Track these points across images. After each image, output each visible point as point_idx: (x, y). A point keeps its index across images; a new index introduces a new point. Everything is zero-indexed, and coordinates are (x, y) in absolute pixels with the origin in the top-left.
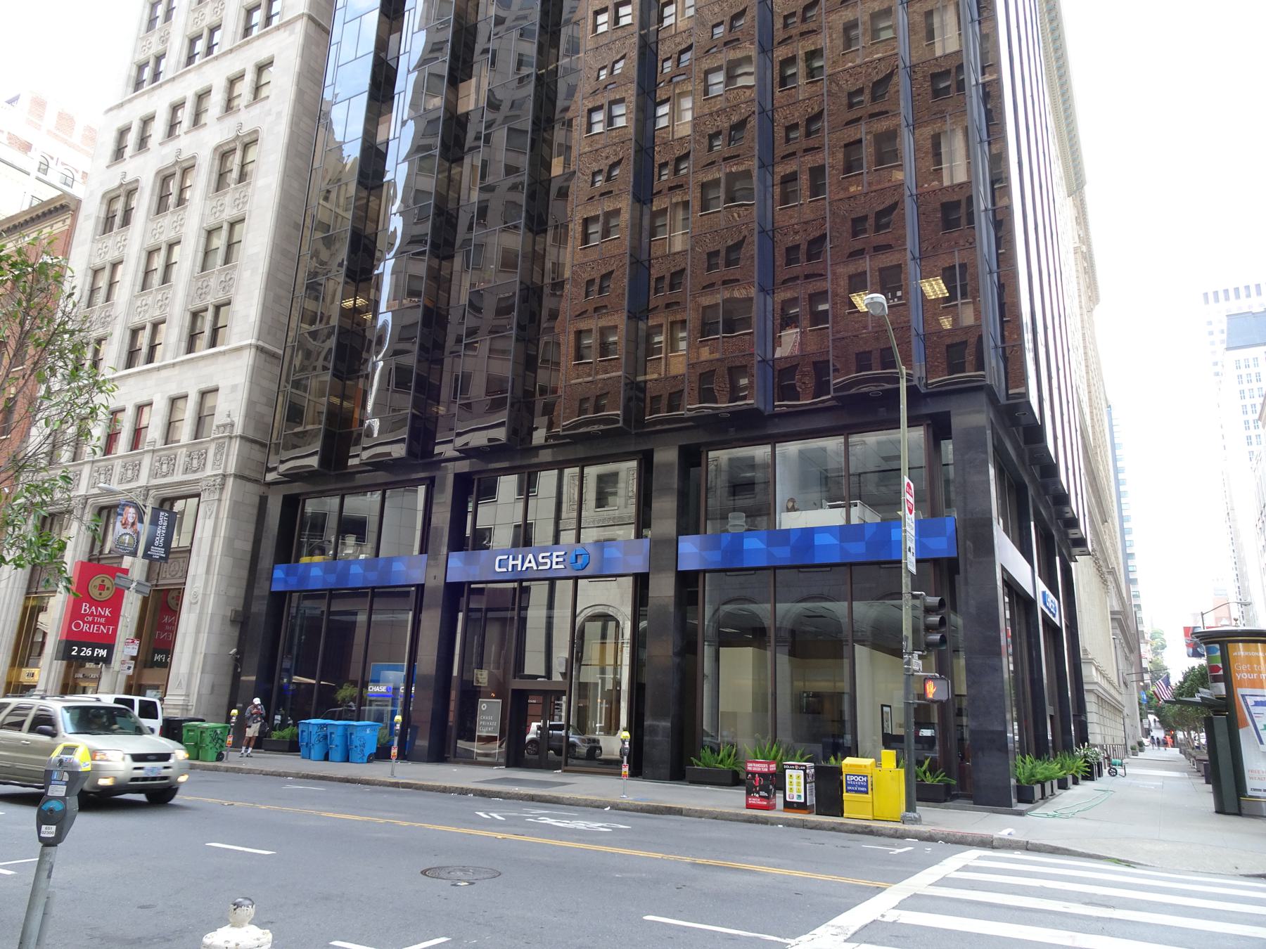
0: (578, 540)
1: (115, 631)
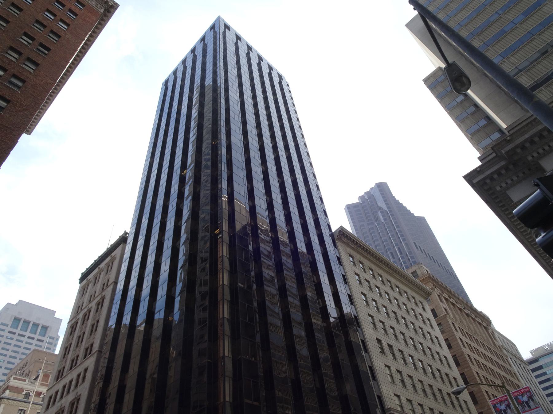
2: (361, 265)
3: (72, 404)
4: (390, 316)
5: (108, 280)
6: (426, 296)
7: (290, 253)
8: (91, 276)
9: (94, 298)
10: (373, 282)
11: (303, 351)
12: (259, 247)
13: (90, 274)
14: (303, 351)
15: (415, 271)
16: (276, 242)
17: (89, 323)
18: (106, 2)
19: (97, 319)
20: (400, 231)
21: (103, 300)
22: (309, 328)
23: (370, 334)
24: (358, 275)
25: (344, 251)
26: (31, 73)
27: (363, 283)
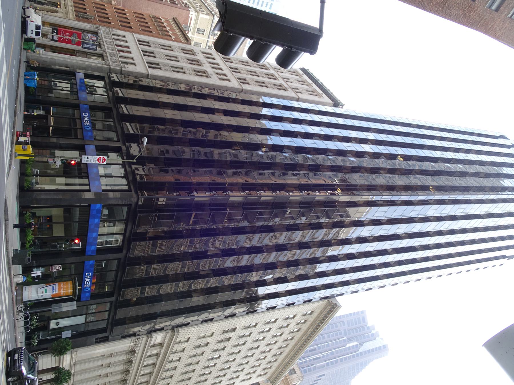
0: (101, 176)
1: (62, 42)
2: (303, 321)
4: (255, 343)
6: (271, 380)
7: (316, 256)
10: (286, 331)
11: (229, 263)
12: (310, 248)
13: (307, 76)
14: (229, 263)
15: (295, 373)
16: (327, 244)
17: (266, 80)
19: (268, 85)
20: (336, 362)
21: (284, 90)
23: (242, 322)
24: (293, 318)
25: (317, 306)
26: (506, 15)
27: (286, 321)
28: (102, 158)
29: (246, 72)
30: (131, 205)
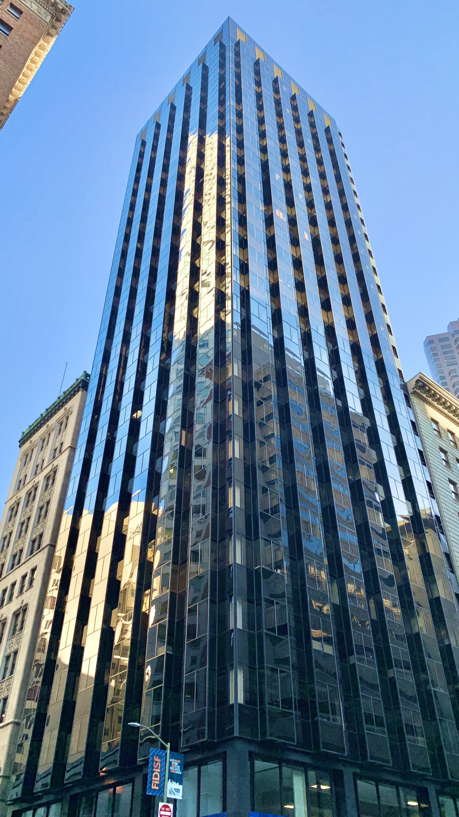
3: (16, 615)
5: (62, 444)
8: (36, 437)
9: (42, 469)
17: (36, 504)
18: (55, 5)
21: (55, 472)
22: (363, 530)
24: (445, 452)
28: (162, 813)
29: (22, 539)
30: (250, 753)
